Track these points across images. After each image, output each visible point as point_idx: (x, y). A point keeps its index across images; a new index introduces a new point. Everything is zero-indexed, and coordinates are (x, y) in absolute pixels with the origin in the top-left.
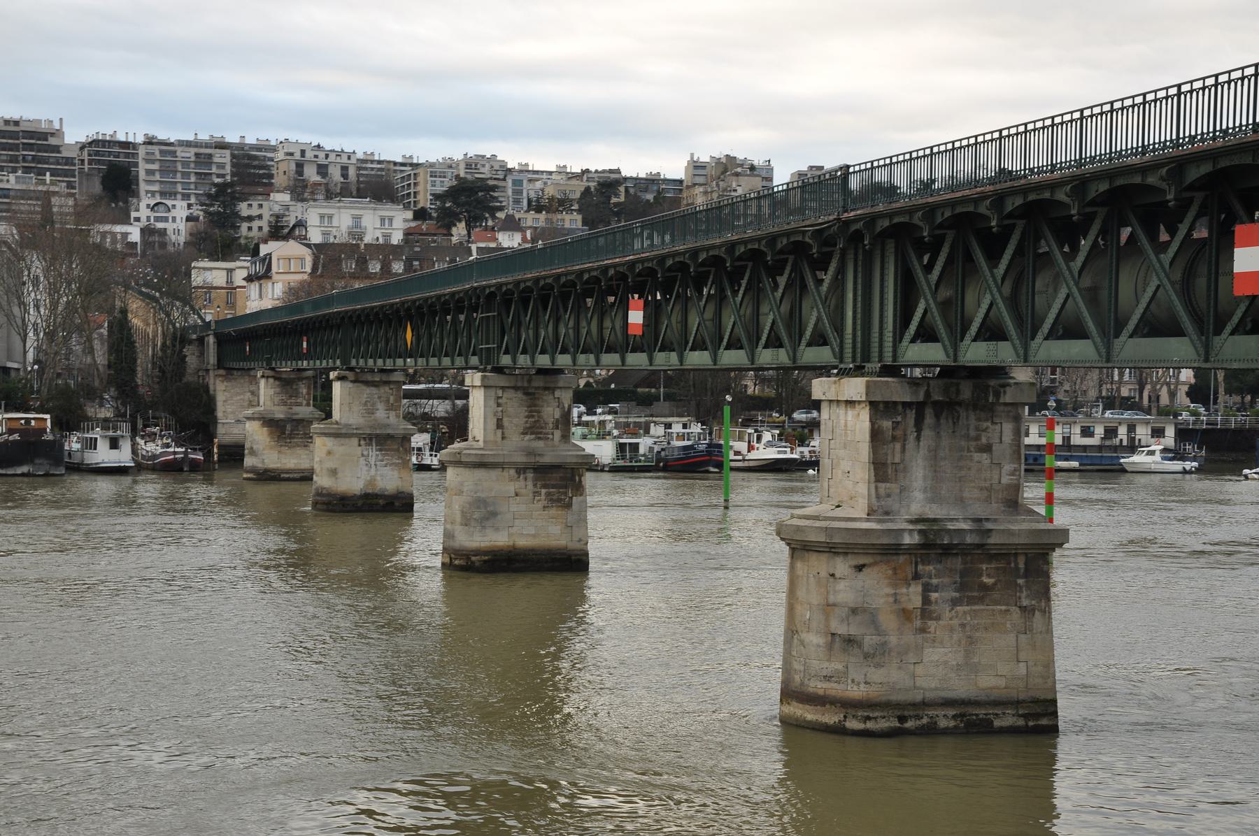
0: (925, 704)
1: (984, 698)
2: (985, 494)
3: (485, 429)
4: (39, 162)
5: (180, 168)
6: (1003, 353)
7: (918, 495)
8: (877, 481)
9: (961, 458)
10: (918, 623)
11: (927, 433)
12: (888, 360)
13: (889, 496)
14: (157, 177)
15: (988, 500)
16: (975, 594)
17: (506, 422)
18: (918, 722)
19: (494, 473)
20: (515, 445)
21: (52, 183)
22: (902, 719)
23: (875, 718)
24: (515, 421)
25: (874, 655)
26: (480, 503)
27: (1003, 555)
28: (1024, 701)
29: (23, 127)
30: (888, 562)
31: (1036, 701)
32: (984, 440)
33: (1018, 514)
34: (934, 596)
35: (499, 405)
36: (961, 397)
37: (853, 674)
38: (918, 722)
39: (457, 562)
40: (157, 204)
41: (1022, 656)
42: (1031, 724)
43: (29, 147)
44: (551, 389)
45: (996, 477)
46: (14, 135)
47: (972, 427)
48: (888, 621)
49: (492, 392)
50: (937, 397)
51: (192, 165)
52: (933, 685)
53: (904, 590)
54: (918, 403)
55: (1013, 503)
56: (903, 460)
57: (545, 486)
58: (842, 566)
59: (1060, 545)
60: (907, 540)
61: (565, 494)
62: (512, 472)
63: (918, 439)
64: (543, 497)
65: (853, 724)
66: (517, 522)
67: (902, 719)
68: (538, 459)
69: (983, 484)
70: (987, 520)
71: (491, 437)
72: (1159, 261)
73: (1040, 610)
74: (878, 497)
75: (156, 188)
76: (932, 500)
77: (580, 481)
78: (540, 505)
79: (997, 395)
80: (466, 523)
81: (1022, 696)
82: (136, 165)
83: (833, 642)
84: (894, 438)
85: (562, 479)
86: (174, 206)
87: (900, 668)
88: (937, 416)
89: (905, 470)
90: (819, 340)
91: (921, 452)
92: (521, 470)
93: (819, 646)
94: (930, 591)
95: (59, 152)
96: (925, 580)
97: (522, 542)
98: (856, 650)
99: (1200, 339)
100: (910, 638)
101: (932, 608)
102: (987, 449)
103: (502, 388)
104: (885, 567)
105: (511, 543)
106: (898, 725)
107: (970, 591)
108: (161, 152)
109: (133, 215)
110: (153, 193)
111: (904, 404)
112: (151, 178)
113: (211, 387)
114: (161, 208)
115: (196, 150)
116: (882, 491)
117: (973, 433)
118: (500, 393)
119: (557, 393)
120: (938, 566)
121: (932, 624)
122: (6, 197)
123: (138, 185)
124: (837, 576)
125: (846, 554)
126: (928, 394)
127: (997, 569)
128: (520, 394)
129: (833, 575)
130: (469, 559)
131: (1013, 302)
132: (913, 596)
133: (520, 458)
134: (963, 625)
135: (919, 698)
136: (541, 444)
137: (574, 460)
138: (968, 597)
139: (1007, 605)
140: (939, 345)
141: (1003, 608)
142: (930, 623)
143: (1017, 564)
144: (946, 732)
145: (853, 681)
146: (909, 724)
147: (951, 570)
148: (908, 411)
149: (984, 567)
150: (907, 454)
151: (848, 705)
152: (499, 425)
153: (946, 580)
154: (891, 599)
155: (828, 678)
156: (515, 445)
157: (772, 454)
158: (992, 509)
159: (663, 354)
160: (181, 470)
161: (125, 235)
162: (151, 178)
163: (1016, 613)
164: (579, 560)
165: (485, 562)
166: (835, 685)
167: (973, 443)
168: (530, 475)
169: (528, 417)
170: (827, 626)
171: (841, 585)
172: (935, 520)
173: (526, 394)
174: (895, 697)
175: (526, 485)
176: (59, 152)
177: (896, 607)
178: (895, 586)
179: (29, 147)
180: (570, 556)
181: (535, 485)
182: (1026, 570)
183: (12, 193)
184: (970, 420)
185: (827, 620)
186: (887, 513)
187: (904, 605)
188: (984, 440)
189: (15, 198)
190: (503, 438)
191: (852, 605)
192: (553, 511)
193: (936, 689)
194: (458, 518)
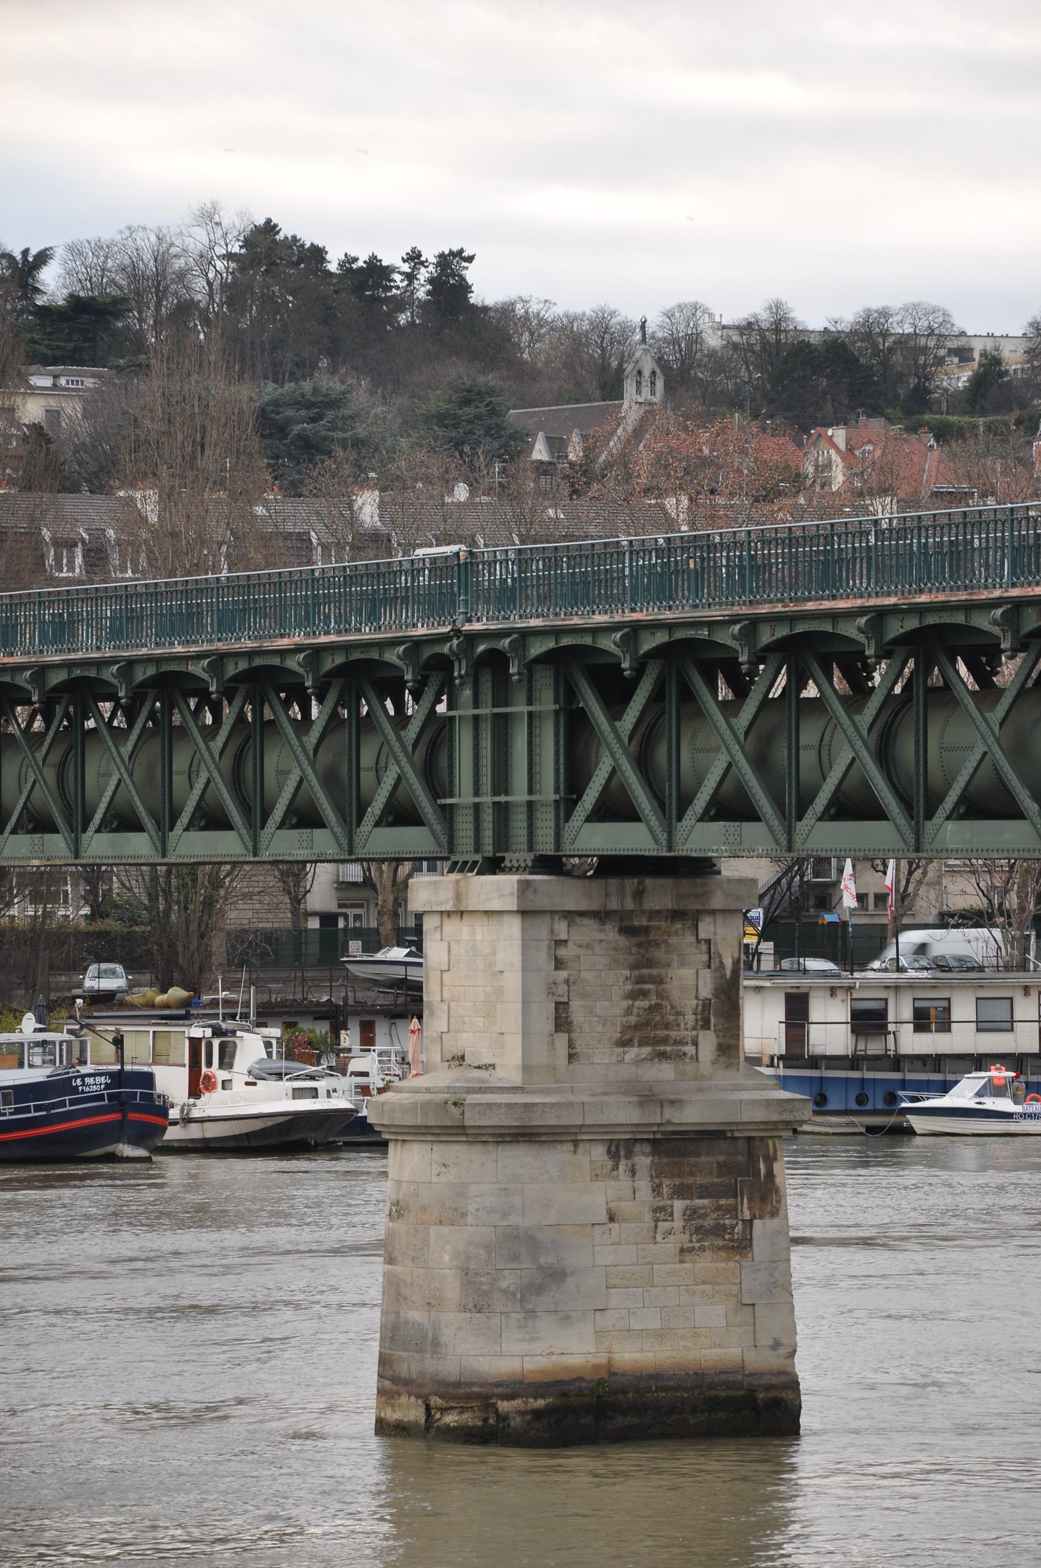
3: (525, 1034)
6: (226, 844)
12: (546, 846)
17: (577, 1011)
20: (604, 1082)
26: (519, 1243)
35: (559, 964)
39: (451, 1419)
44: (687, 917)
49: (542, 929)
57: (681, 1192)
61: (733, 1211)
62: (599, 1152)
64: (678, 1223)
66: (616, 1297)
68: (670, 1114)
71: (541, 1057)
72: (209, 749)
77: (770, 1175)
78: (671, 1246)
80: (478, 1301)
85: (724, 1169)
90: (402, 814)
92: (620, 1147)
97: (634, 1355)
99: (158, 835)
103: (569, 915)
105: (602, 1359)
118: (562, 929)
119: (706, 928)
128: (610, 933)
131: (236, 781)
133: (624, 1114)
136: (665, 1072)
137: (760, 1115)
140: (145, 835)
152: (562, 1022)
156: (604, 1082)
157: (276, 1099)
159: (106, 837)
164: (776, 1404)
165: (537, 1414)
168: (644, 1161)
169: (633, 996)
173: (627, 931)
175: (633, 1189)
180: (752, 1391)
181: (657, 1190)
190: (572, 1057)
192: (706, 1263)
194: (452, 1290)
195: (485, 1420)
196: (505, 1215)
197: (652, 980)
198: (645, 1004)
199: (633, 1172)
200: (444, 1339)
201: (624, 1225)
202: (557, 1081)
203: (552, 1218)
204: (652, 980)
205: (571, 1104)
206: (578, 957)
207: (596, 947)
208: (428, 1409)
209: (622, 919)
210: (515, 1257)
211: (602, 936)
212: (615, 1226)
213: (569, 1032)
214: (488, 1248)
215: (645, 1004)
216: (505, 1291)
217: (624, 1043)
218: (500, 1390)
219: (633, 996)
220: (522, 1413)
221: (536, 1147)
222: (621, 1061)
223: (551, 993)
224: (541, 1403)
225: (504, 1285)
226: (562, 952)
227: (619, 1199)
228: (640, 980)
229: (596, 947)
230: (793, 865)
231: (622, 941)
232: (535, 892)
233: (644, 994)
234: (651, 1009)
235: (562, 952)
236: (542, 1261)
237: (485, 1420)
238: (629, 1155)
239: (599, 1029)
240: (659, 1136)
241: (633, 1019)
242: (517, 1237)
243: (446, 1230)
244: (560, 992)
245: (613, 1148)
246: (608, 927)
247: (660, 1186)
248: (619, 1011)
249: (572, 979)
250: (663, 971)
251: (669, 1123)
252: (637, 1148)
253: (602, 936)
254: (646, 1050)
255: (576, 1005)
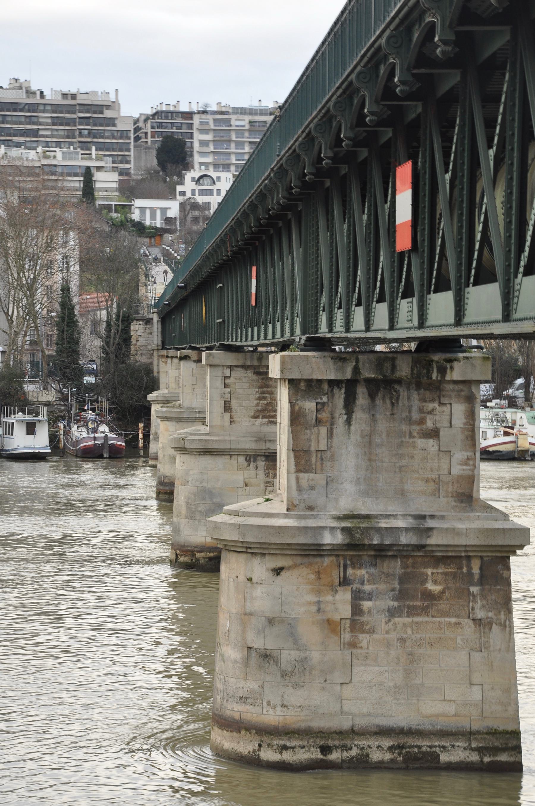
0: (353, 733)
1: (429, 727)
2: (432, 486)
4: (95, 137)
5: (234, 138)
7: (349, 487)
8: (298, 471)
9: (401, 445)
10: (347, 636)
11: (359, 415)
13: (312, 488)
14: (211, 148)
15: (436, 493)
16: (418, 603)
17: (234, 404)
18: (346, 754)
19: (221, 461)
21: (98, 159)
22: (325, 750)
23: (293, 748)
24: (245, 403)
25: (292, 673)
27: (451, 558)
28: (478, 732)
29: (81, 100)
30: (311, 564)
31: (493, 733)
32: (430, 424)
33: (472, 510)
34: (366, 605)
35: (226, 386)
36: (398, 374)
37: (270, 695)
38: (346, 754)
39: (182, 559)
40: (202, 177)
41: (476, 679)
42: (487, 759)
43: (84, 120)
45: (445, 467)
46: (70, 109)
47: (415, 409)
48: (310, 634)
49: (219, 372)
50: (368, 373)
51: (247, 134)
52: (365, 710)
53: (329, 598)
54: (348, 380)
55: (466, 496)
56: (329, 447)
58: (259, 569)
59: (521, 547)
60: (328, 539)
62: (242, 459)
63: (348, 422)
65: (268, 755)
67: (325, 750)
69: (429, 475)
70: (432, 517)
73: (500, 624)
74: (300, 489)
75: (209, 159)
76: (366, 494)
79: (442, 371)
81: (475, 727)
82: (191, 136)
83: (249, 657)
84: (319, 422)
86: (219, 178)
87: (323, 689)
88: (372, 396)
89: (332, 458)
91: (353, 437)
93: (236, 661)
94: (362, 599)
95: (114, 125)
96: (355, 586)
98: (273, 668)
100: (336, 654)
101: (365, 618)
102: (434, 434)
103: (231, 367)
104: (304, 571)
106: (320, 756)
107: (411, 599)
108: (215, 120)
109: (179, 188)
110: (206, 165)
111: (331, 383)
112: (205, 149)
113: (155, 369)
114: (206, 181)
115: (251, 118)
116: (304, 483)
117: (415, 416)
118: (227, 372)
120: (372, 570)
121: (364, 639)
122: (53, 174)
123: (192, 156)
124: (255, 580)
125: (263, 554)
126: (356, 370)
127: (446, 574)
128: (250, 374)
129: (250, 580)
130: (194, 555)
132: (341, 603)
133: (250, 445)
134: (403, 640)
135: (346, 725)
138: (409, 607)
139: (458, 616)
141: (453, 620)
142: (361, 636)
143: (470, 568)
144: (380, 766)
145: (269, 703)
146: (335, 756)
147: (388, 575)
148: (336, 391)
149: (429, 571)
150: (335, 440)
151: (264, 732)
153: (382, 587)
154: (314, 608)
155: (243, 699)
158: (442, 504)
160: (101, 457)
161: (164, 210)
162: (205, 149)
163: (468, 625)
166: (249, 708)
167: (416, 428)
169: (259, 399)
170: (244, 639)
171: (258, 591)
172: (367, 517)
174: (318, 724)
176: (114, 125)
177: (320, 617)
178: (318, 592)
179: (84, 120)
182: (482, 576)
183: (59, 170)
184: (412, 400)
185: (244, 632)
186: (311, 508)
187: (329, 616)
188: (430, 424)
189: (62, 174)
190: (231, 422)
191: (268, 615)
193: (369, 714)
195: (192, 560)
196: (201, 482)
197: (268, 393)
198: (265, 402)
199: (257, 467)
200: (181, 529)
201: (251, 488)
202: (225, 431)
203: (219, 484)
204: (268, 393)
205: (225, 440)
206: (235, 383)
207: (243, 379)
208: (177, 555)
209: (255, 369)
210: (204, 499)
211: (246, 375)
212: (248, 488)
213: (231, 412)
214: (195, 495)
215: (265, 402)
216: (200, 512)
217: (255, 417)
218: (197, 549)
219: (259, 399)
220: (204, 558)
221: (214, 457)
222: (254, 424)
223: (222, 397)
224: (212, 555)
225: (200, 509)
226: (227, 381)
227: (250, 478)
228: (263, 393)
229: (243, 379)
230: (51, 242)
231: (255, 377)
232: (213, 357)
233: (265, 398)
234: (267, 404)
235: (227, 381)
236: (214, 501)
237: (192, 560)
238: (255, 461)
239: (244, 411)
240: (267, 454)
241: (259, 408)
242: (205, 491)
243: (183, 487)
244: (226, 396)
245: (248, 458)
246: (249, 371)
247: (268, 473)
248: (253, 405)
249: (232, 392)
250: (273, 389)
251: (269, 449)
252: (259, 458)
253: (246, 375)
254: (265, 420)
255: (233, 402)
